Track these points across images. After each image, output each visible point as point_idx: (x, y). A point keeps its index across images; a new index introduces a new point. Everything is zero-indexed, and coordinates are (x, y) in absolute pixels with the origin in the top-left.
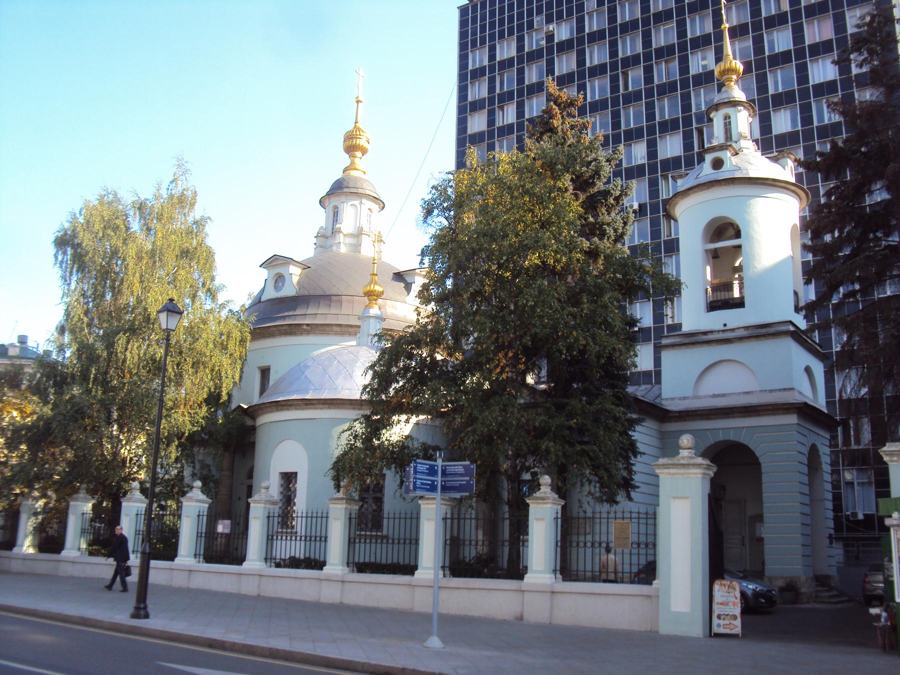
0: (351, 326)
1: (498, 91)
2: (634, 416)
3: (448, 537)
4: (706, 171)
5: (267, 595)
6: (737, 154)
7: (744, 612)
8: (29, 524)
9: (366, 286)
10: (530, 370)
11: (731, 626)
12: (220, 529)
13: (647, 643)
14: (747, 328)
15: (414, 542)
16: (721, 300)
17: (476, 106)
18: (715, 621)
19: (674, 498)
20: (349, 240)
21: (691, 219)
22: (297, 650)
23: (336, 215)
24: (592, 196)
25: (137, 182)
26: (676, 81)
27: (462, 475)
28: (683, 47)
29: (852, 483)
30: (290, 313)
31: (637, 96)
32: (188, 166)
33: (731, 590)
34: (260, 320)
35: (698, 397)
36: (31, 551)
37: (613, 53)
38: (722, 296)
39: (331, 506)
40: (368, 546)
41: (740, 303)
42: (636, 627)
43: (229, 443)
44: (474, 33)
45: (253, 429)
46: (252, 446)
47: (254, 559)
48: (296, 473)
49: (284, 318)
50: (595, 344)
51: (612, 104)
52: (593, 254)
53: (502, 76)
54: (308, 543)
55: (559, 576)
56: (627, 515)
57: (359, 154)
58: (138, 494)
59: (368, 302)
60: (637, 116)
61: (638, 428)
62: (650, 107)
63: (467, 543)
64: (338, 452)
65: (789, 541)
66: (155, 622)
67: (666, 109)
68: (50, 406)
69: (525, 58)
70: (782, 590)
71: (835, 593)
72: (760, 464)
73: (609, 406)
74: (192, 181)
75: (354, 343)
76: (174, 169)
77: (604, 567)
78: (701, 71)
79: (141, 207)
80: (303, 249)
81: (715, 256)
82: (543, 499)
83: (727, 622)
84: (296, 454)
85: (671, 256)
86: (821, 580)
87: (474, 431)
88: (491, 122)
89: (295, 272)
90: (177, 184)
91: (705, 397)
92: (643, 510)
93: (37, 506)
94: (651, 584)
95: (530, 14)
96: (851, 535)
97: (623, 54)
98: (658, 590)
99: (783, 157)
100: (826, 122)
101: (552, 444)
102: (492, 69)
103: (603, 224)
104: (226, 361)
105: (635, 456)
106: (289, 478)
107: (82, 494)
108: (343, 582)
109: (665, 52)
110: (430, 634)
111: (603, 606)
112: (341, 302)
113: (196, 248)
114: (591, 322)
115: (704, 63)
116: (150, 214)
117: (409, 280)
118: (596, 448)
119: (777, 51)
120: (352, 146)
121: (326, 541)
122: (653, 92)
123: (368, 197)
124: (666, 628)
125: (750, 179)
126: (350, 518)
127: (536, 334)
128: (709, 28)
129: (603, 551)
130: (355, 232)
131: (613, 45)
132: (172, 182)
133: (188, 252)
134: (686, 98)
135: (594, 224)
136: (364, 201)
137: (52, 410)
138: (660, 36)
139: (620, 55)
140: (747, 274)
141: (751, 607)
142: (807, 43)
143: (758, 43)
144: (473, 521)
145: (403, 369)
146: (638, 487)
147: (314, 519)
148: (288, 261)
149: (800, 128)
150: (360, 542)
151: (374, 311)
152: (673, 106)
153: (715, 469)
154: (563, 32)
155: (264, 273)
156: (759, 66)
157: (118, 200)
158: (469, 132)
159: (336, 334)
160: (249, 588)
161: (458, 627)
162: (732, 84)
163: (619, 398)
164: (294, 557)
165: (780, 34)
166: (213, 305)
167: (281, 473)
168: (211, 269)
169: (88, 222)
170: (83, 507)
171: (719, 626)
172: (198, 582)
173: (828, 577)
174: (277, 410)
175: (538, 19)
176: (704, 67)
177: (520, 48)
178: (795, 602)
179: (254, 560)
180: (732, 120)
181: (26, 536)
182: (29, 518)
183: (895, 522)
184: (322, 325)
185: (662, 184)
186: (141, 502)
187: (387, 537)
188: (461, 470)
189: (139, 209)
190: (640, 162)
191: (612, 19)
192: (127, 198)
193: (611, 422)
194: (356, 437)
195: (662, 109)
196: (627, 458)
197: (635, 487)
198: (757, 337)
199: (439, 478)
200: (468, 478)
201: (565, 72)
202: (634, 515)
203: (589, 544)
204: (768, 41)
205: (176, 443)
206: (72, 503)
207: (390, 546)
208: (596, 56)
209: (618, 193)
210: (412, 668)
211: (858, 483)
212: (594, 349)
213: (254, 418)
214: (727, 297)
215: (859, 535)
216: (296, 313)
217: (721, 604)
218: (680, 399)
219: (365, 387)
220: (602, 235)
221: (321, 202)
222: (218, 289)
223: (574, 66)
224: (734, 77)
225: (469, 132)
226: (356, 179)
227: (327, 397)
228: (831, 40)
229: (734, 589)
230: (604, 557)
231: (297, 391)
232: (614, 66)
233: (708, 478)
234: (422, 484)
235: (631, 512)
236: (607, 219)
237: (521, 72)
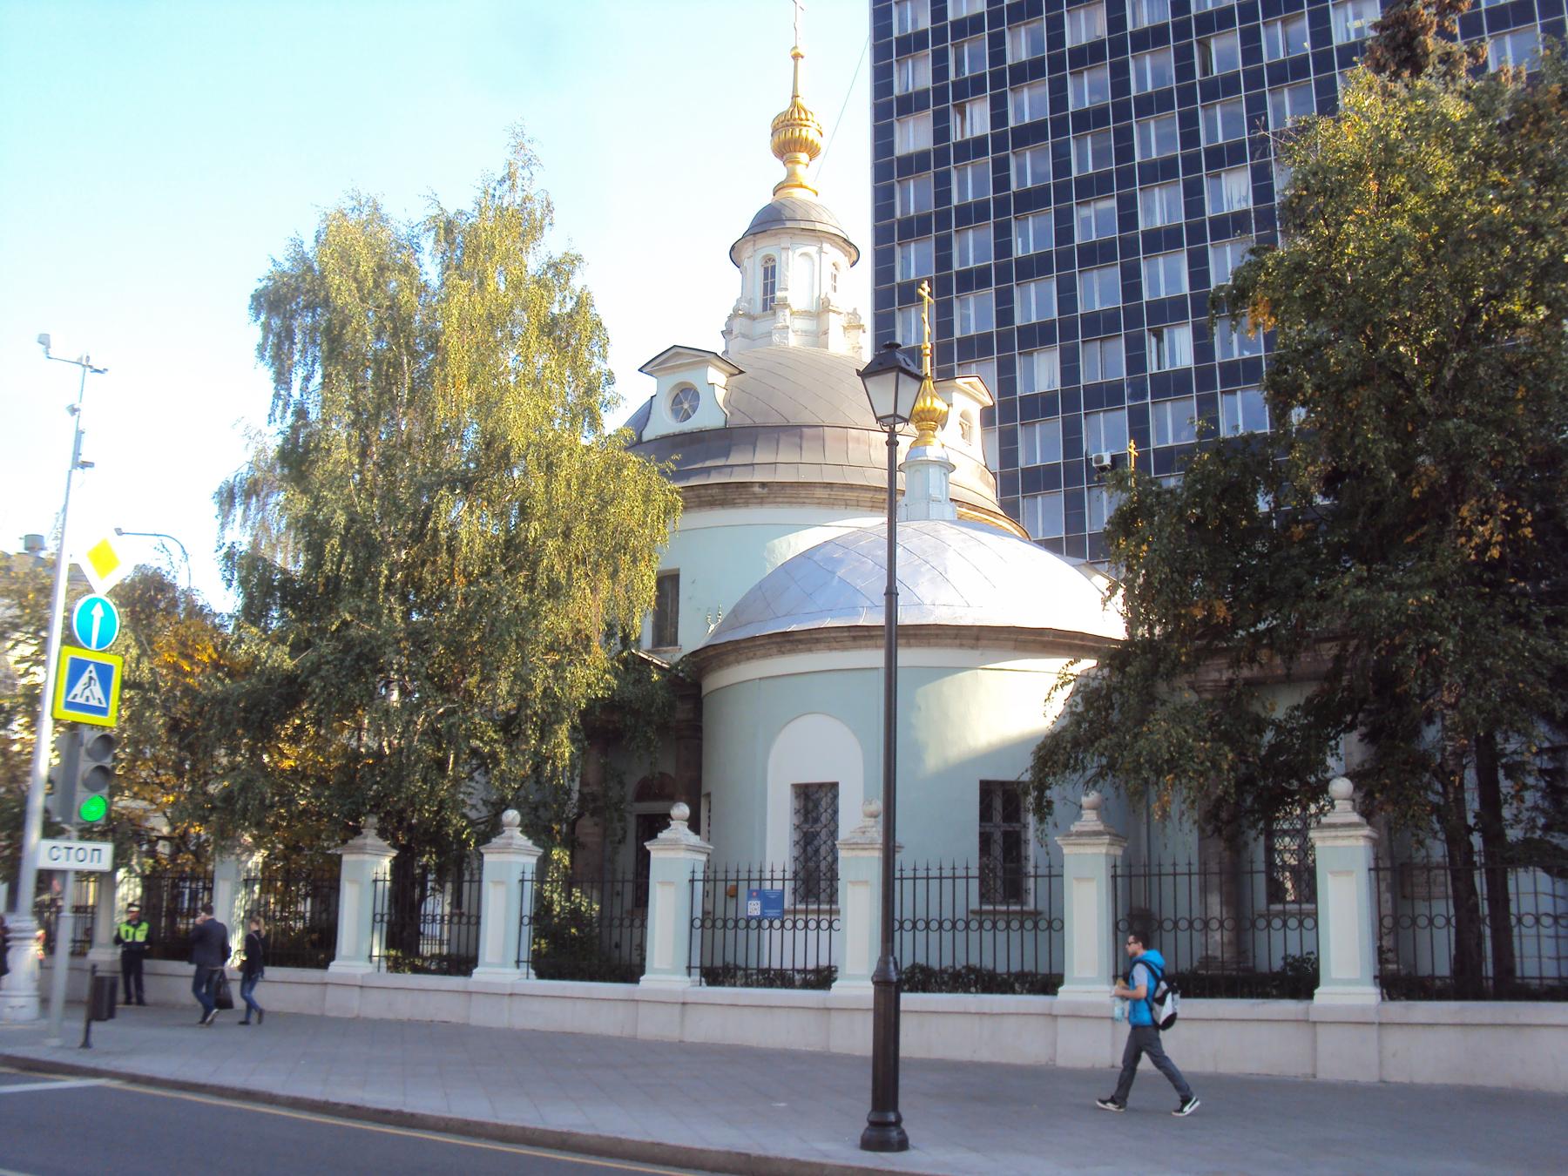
3: (698, 913)
8: (237, 903)
17: (910, 104)
20: (800, 324)
22: (550, 1128)
25: (418, 181)
31: (1229, 85)
40: (988, 936)
48: (834, 786)
49: (707, 471)
57: (803, 157)
63: (1168, 925)
74: (539, 184)
78: (1353, 39)
79: (447, 229)
88: (941, 134)
102: (939, 35)
107: (371, 838)
121: (478, 923)
126: (1114, 877)
130: (813, 309)
136: (826, 247)
144: (1195, 879)
148: (701, 357)
157: (377, 216)
159: (820, 503)
160: (655, 1026)
172: (373, 1007)
182: (237, 892)
187: (1036, 914)
190: (1237, 208)
192: (407, 212)
195: (1279, 109)
206: (347, 859)
237: (997, 42)
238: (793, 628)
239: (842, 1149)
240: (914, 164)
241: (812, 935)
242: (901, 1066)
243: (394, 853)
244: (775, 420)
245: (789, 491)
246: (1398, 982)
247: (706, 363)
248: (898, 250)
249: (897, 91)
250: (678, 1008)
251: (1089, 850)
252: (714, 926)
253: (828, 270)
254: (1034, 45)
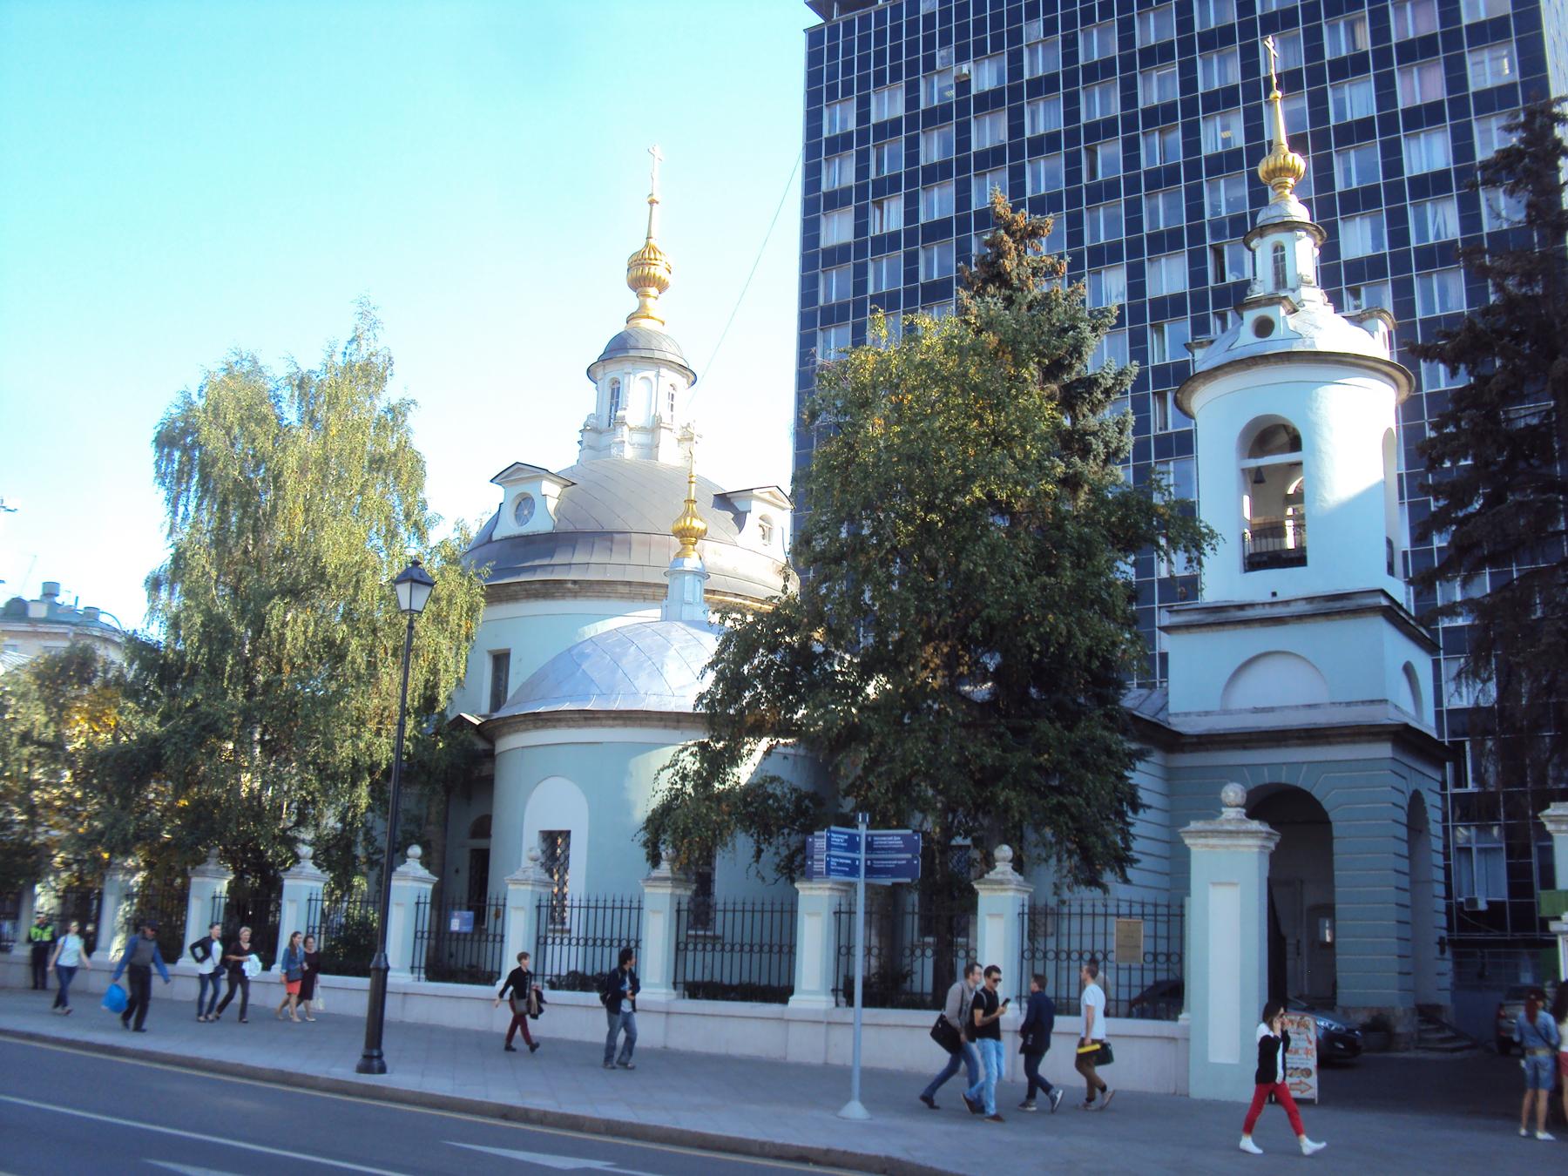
1: (873, 175)
2: (1134, 746)
4: (1245, 339)
6: (1295, 311)
9: (678, 520)
11: (1303, 1087)
14: (1310, 600)
15: (787, 949)
17: (835, 200)
19: (1214, 884)
20: (638, 438)
21: (1218, 414)
26: (1178, 165)
27: (898, 851)
28: (1190, 108)
29: (1469, 850)
30: (545, 562)
31: (1111, 189)
32: (378, 314)
33: (1302, 1029)
34: (498, 572)
35: (1226, 712)
37: (1072, 115)
38: (1269, 545)
39: (647, 890)
41: (1297, 559)
42: (1151, 1088)
43: (450, 782)
44: (833, 75)
45: (490, 755)
46: (488, 783)
48: (568, 833)
49: (534, 569)
51: (1073, 200)
52: (1071, 483)
53: (879, 149)
54: (590, 950)
57: (653, 291)
58: (309, 866)
60: (1111, 222)
61: (1140, 765)
62: (1134, 208)
64: (656, 802)
65: (1378, 955)
66: (403, 1076)
67: (1161, 212)
68: (157, 718)
69: (919, 120)
70: (1365, 1028)
71: (1448, 1033)
73: (1099, 732)
78: (1220, 149)
79: (302, 384)
80: (559, 452)
81: (1257, 478)
82: (1001, 882)
86: (1427, 1013)
88: (861, 228)
89: (551, 492)
90: (359, 346)
91: (1240, 711)
92: (1162, 900)
93: (132, 882)
94: (1176, 1019)
96: (1466, 936)
98: (1187, 1029)
99: (1371, 317)
100: (1432, 241)
101: (1013, 794)
102: (863, 137)
103: (1086, 433)
104: (445, 643)
105: (1135, 811)
106: (555, 844)
107: (211, 866)
108: (668, 1013)
109: (1160, 116)
110: (848, 1100)
114: (1080, 597)
115: (1226, 134)
116: (316, 397)
117: (741, 506)
118: (1081, 802)
119: (1349, 119)
120: (641, 279)
121: (502, 941)
122: (1138, 183)
123: (669, 364)
124: (1200, 1090)
126: (678, 911)
127: (989, 618)
128: (1235, 76)
131: (1072, 101)
133: (382, 459)
134: (1195, 196)
135: (1070, 433)
136: (664, 371)
137: (160, 724)
138: (1218, 189)
139: (1083, 119)
140: (1310, 509)
141: (1332, 1055)
142: (1400, 106)
145: (768, 666)
146: (1138, 861)
148: (540, 473)
149: (1386, 250)
150: (714, 949)
151: (691, 563)
152: (1171, 208)
153: (1277, 839)
154: (985, 76)
155: (498, 494)
156: (1320, 138)
157: (257, 370)
159: (622, 597)
162: (1287, 192)
163: (1111, 718)
164: (576, 972)
165: (1354, 89)
167: (543, 833)
169: (216, 408)
173: (1438, 1008)
174: (536, 728)
175: (944, 53)
176: (1226, 142)
177: (912, 102)
179: (655, 986)
180: (1287, 253)
181: (115, 934)
182: (119, 903)
185: (1152, 339)
186: (317, 879)
187: (715, 937)
189: (300, 387)
191: (1070, 56)
192: (277, 369)
194: (684, 778)
195: (1154, 213)
196: (1121, 815)
198: (1327, 615)
200: (909, 856)
202: (1161, 910)
203: (1051, 955)
204: (1335, 101)
206: (195, 880)
208: (1043, 118)
209: (1110, 382)
210: (825, 1147)
211: (1480, 851)
213: (491, 741)
214: (1277, 548)
215: (1477, 936)
216: (556, 560)
218: (1199, 714)
219: (701, 697)
220: (1085, 452)
222: (431, 522)
223: (1003, 136)
224: (1291, 181)
226: (649, 334)
227: (622, 708)
228: (1442, 102)
229: (1307, 1028)
231: (569, 697)
232: (1072, 137)
233: (1267, 851)
234: (839, 864)
235: (1156, 905)
236: (1092, 422)
237: (912, 144)
238: (541, 710)
239: (344, 1070)
240: (836, 256)
241: (565, 949)
243: (231, 877)
244: (592, 527)
245: (597, 588)
247: (541, 478)
248: (820, 335)
249: (824, 188)
252: (723, 950)
254: (946, 149)
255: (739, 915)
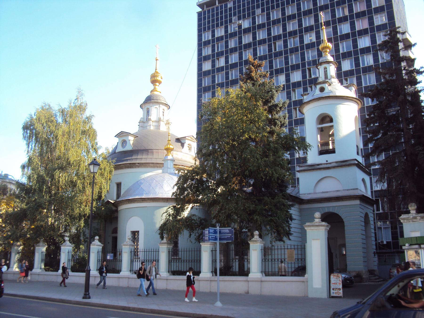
0: (158, 163)
1: (216, 51)
2: (291, 203)
4: (317, 93)
5: (132, 286)
6: (330, 85)
7: (344, 286)
9: (166, 146)
10: (244, 184)
11: (338, 293)
12: (108, 258)
13: (304, 301)
16: (325, 151)
17: (206, 58)
18: (332, 291)
19: (313, 239)
20: (154, 124)
21: (311, 113)
23: (148, 112)
24: (270, 107)
28: (301, 31)
29: (381, 228)
30: (130, 158)
31: (280, 54)
32: (83, 92)
33: (338, 278)
34: (117, 161)
35: (316, 193)
36: (17, 270)
37: (269, 34)
38: (325, 148)
41: (333, 151)
42: (298, 295)
43: (106, 219)
44: (205, 24)
45: (117, 211)
46: (116, 218)
47: (125, 271)
48: (138, 231)
49: (127, 160)
50: (276, 173)
51: (270, 57)
52: (272, 133)
55: (263, 274)
56: (289, 247)
57: (157, 84)
58: (68, 243)
59: (166, 153)
60: (281, 62)
61: (292, 208)
62: (286, 58)
64: (162, 222)
67: (294, 59)
68: (25, 204)
69: (228, 36)
70: (355, 277)
71: (377, 277)
72: (343, 222)
74: (84, 99)
75: (160, 171)
76: (77, 93)
77: (280, 269)
79: (63, 111)
80: (133, 128)
81: (321, 130)
82: (256, 241)
83: (337, 291)
84: (141, 224)
85: (297, 127)
86: (371, 272)
87: (225, 212)
88: (213, 66)
89: (131, 139)
91: (319, 193)
93: (19, 249)
94: (304, 276)
95: (230, 15)
96: (381, 251)
97: (274, 34)
98: (307, 279)
99: (351, 86)
101: (258, 217)
102: (213, 41)
103: (275, 119)
104: (103, 181)
105: (291, 221)
106: (135, 234)
107: (41, 244)
108: (167, 279)
109: (293, 34)
111: (286, 286)
112: (148, 152)
113: (88, 130)
115: (311, 38)
117: (183, 142)
120: (154, 80)
122: (287, 52)
123: (162, 104)
124: (311, 295)
125: (337, 96)
126: (169, 252)
128: (312, 23)
129: (279, 262)
131: (269, 30)
132: (76, 100)
133: (85, 131)
134: (303, 55)
135: (271, 119)
136: (161, 106)
137: (26, 205)
138: (290, 26)
139: (272, 35)
140: (336, 138)
141: (346, 284)
142: (357, 30)
143: (335, 30)
145: (191, 185)
146: (293, 234)
147: (148, 252)
148: (128, 134)
149: (354, 68)
150: (174, 262)
151: (170, 157)
152: (297, 58)
153: (330, 227)
154: (246, 24)
155: (117, 140)
156: (336, 39)
157: (50, 108)
158: (203, 70)
159: (151, 167)
161: (227, 298)
162: (327, 53)
163: (284, 196)
165: (344, 25)
166: (96, 156)
167: (132, 232)
168: (95, 139)
169: (39, 119)
170: (41, 249)
171: (334, 293)
172: (41, 279)
175: (234, 18)
176: (311, 40)
177: (226, 31)
178: (361, 282)
179: (255, 273)
181: (14, 263)
182: (16, 255)
183: (407, 248)
184: (145, 163)
185: (292, 94)
186: (70, 246)
187: (179, 259)
188: (227, 231)
189: (62, 112)
191: (268, 18)
192: (55, 108)
193: (282, 207)
194: (169, 215)
195: (292, 60)
196: (288, 222)
197: (291, 234)
198: (341, 166)
199: (218, 235)
200: (231, 235)
201: (247, 43)
203: (270, 260)
204: (339, 29)
205: (84, 219)
206: (37, 248)
207: (183, 263)
208: (262, 35)
209: (281, 105)
210: (210, 314)
211: (384, 228)
212: (276, 175)
216: (132, 158)
217: (334, 284)
218: (308, 194)
219: (173, 193)
220: (275, 124)
221: (141, 106)
223: (251, 40)
224: (328, 50)
225: (203, 70)
226: (157, 96)
227: (152, 197)
229: (339, 277)
230: (280, 265)
232: (270, 40)
234: (212, 238)
236: (277, 116)
237: (227, 42)
240: (207, 73)
242: (90, 287)
243: (47, 247)
244: (143, 148)
245: (144, 165)
246: (214, 272)
248: (203, 95)
250: (259, 283)
251: (164, 246)
253: (161, 111)
254: (236, 44)
255: (150, 252)
